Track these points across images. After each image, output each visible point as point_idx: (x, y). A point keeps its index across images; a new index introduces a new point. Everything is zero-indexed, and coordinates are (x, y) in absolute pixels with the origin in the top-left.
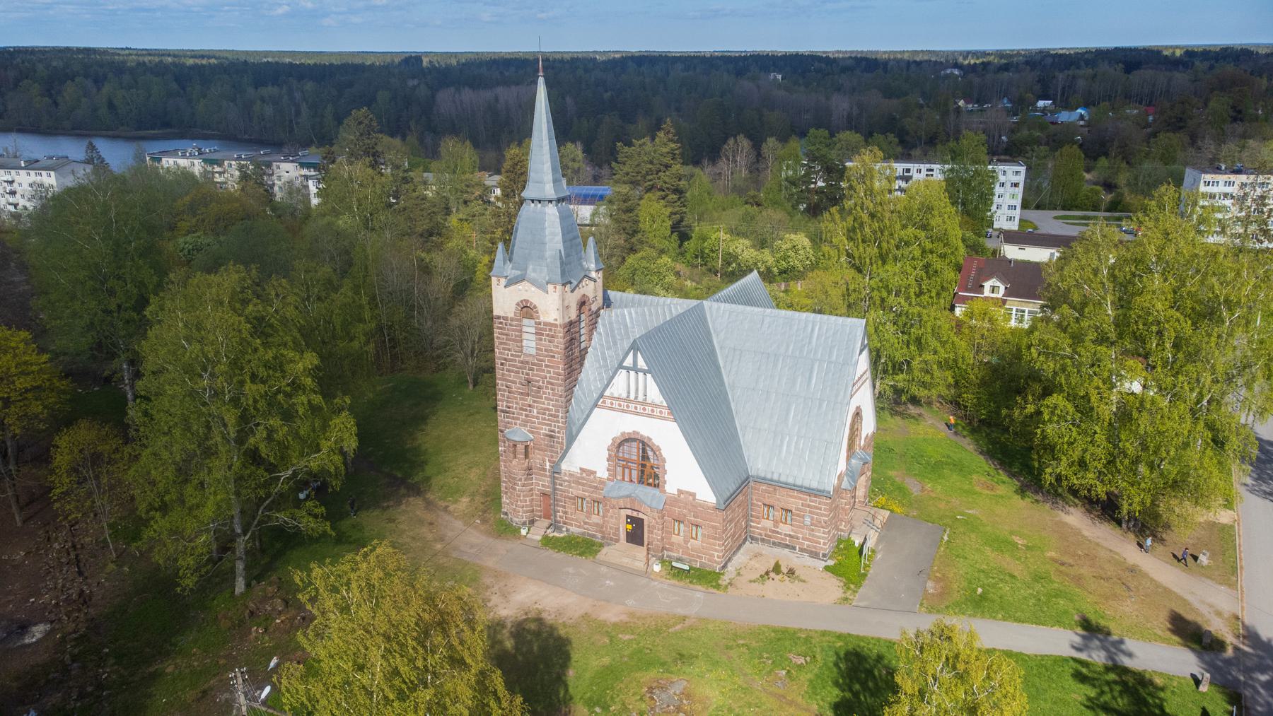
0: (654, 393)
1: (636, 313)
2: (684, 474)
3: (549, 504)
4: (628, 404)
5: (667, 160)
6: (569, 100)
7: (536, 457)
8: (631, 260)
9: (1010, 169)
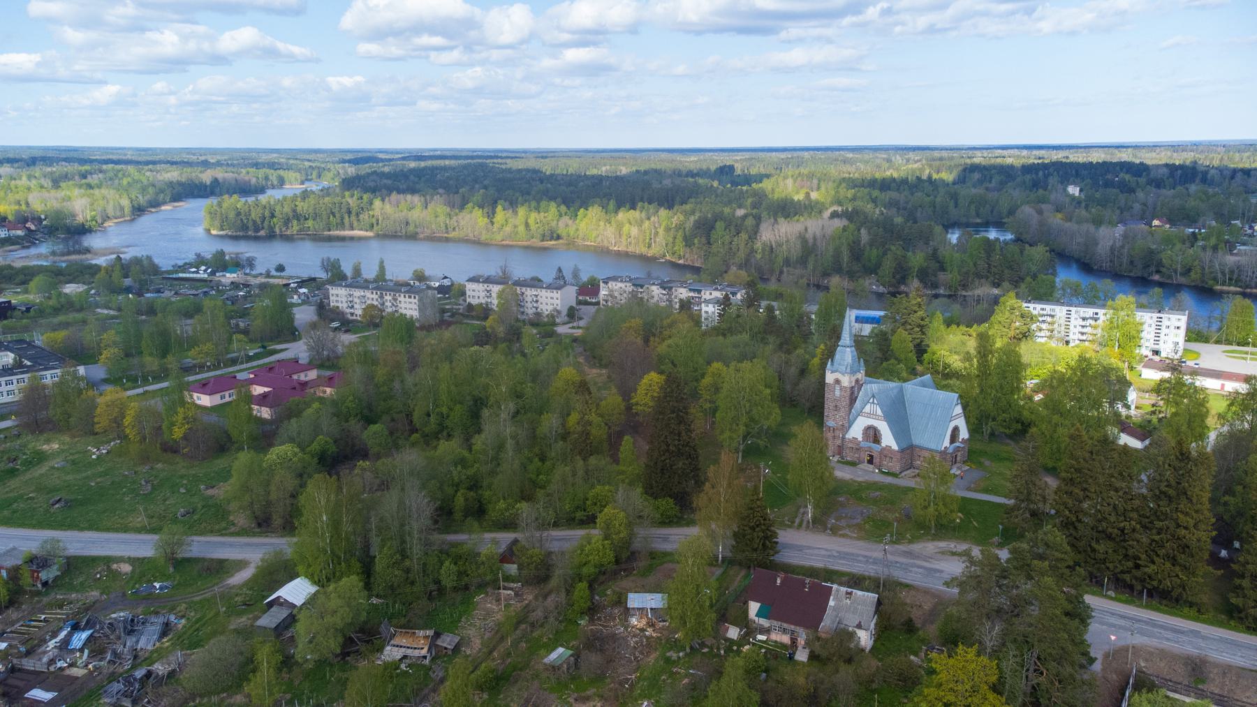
0: (879, 412)
1: (874, 386)
2: (888, 440)
3: (840, 450)
4: (869, 415)
5: (916, 308)
6: (863, 231)
7: (837, 433)
8: (885, 364)
9: (1174, 317)
